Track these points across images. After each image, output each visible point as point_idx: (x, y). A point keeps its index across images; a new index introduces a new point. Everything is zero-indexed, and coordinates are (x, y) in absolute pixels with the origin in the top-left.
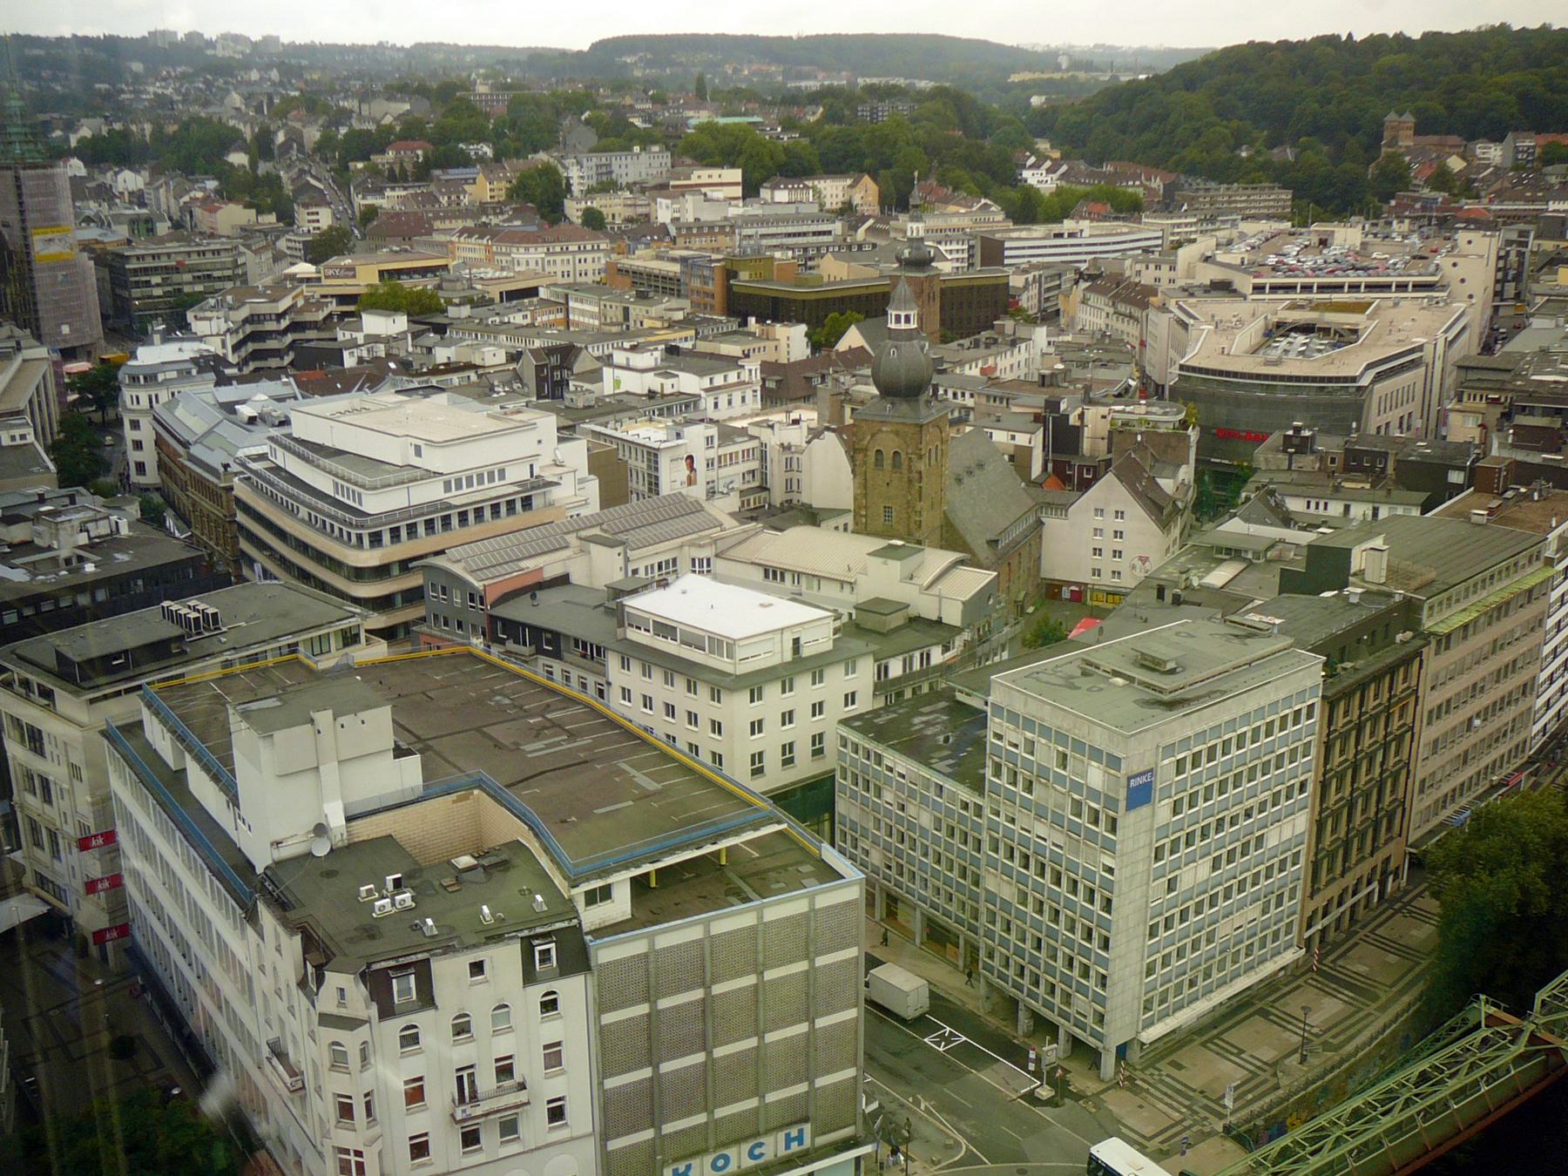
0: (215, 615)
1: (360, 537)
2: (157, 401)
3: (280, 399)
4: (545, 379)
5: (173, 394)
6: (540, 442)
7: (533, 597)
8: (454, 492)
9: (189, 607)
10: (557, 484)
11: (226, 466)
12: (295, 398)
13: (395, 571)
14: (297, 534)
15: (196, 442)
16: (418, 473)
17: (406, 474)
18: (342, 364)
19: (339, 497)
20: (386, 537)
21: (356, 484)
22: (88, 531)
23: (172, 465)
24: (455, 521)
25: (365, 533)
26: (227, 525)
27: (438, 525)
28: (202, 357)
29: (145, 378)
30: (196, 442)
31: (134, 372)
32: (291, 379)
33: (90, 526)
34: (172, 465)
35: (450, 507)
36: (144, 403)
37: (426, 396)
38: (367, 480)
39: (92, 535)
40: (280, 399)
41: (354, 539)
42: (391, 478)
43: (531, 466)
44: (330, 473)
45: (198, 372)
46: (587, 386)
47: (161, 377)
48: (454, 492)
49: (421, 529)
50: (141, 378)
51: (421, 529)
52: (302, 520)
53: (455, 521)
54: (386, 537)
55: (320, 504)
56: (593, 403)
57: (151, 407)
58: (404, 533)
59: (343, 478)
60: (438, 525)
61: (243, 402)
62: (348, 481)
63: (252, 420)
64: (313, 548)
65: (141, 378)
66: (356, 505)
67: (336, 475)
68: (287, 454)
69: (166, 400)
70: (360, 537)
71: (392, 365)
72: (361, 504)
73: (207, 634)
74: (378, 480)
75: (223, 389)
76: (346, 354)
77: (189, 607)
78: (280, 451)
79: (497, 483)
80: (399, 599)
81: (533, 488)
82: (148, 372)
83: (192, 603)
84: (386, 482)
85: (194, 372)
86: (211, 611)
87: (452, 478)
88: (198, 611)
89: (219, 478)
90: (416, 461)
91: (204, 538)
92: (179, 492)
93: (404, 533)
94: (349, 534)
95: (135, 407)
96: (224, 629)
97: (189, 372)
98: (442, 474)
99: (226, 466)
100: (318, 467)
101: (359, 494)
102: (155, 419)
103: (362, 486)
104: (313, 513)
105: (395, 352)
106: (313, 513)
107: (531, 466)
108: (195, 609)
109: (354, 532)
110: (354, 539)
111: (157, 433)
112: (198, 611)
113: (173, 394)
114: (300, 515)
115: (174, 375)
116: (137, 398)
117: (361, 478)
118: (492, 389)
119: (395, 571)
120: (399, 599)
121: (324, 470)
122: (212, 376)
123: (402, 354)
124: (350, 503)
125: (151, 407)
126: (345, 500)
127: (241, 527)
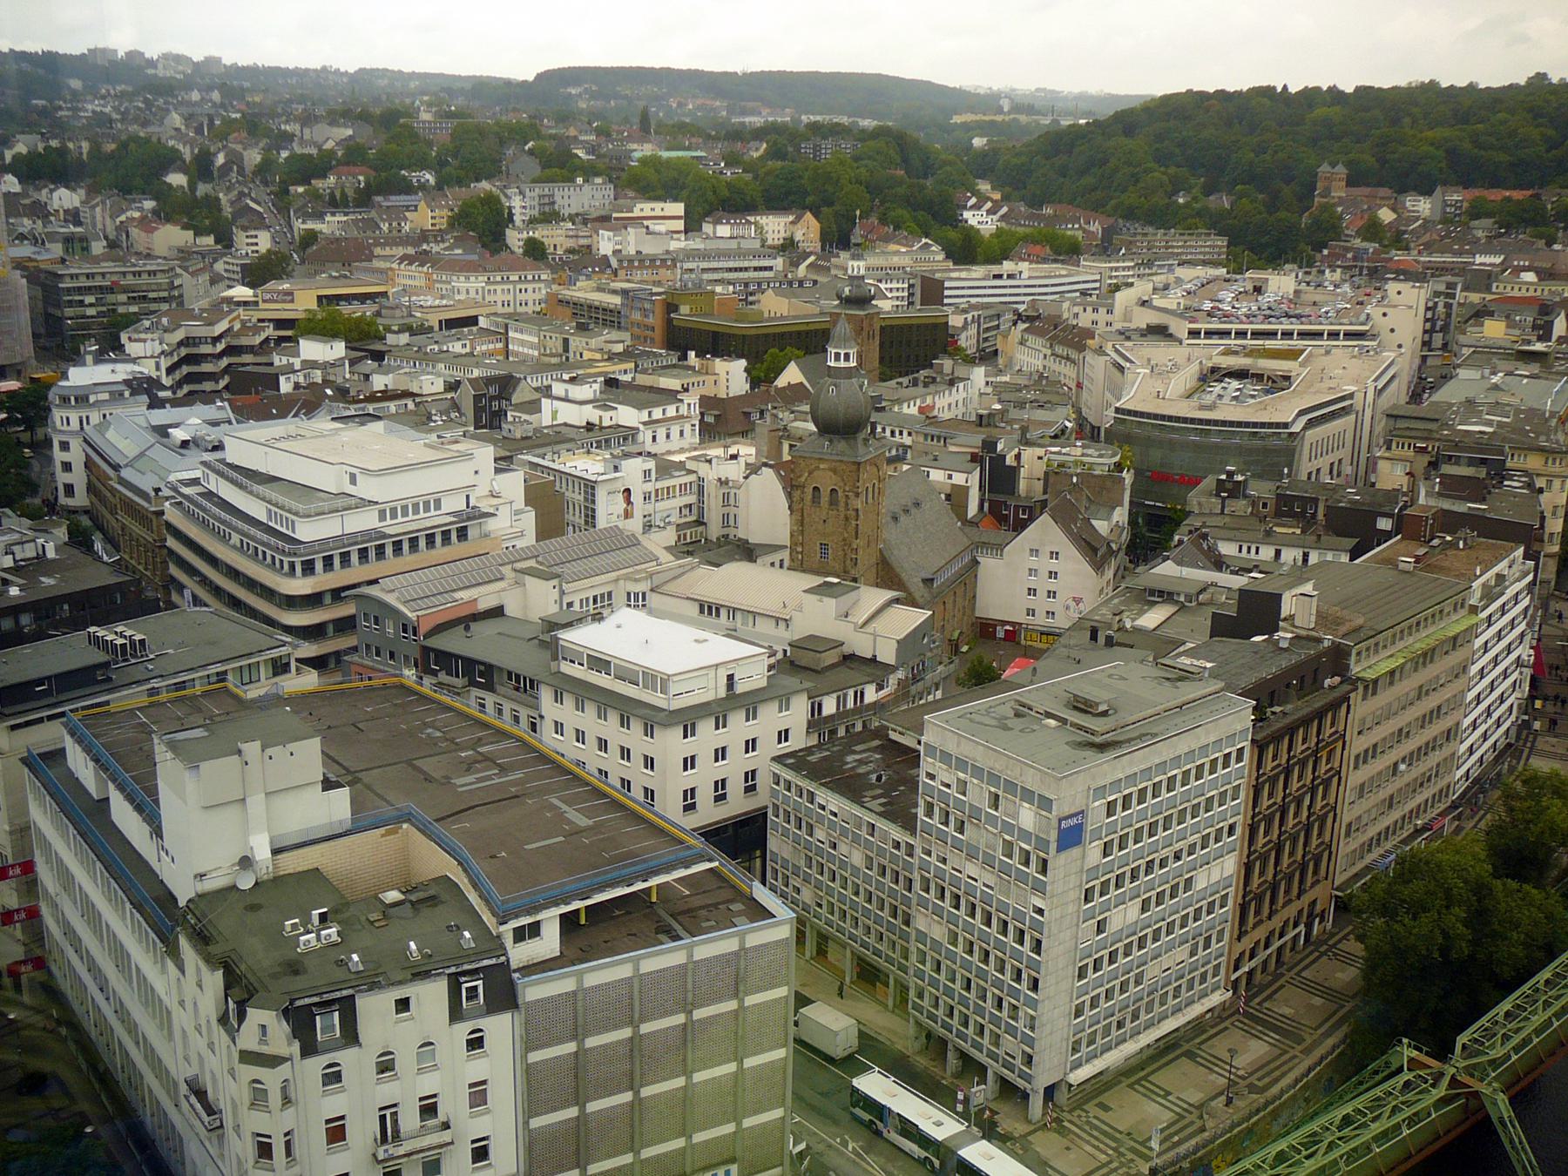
0: (142, 642)
1: (292, 566)
2: (88, 423)
3: (215, 424)
4: (483, 409)
5: (104, 416)
6: (476, 472)
7: (467, 628)
8: (389, 522)
9: (116, 633)
10: (494, 515)
11: (157, 490)
12: (230, 422)
13: (328, 599)
14: (229, 562)
15: (126, 466)
16: (353, 501)
17: (340, 503)
18: (278, 390)
19: (272, 524)
20: (319, 566)
21: (289, 511)
22: (13, 554)
23: (103, 489)
24: (389, 550)
25: (298, 560)
26: (157, 550)
27: (372, 554)
28: (135, 378)
29: (76, 399)
30: (126, 466)
31: (65, 393)
32: (226, 403)
33: (16, 549)
34: (103, 489)
35: (385, 536)
36: (75, 425)
37: (362, 424)
38: (301, 507)
39: (18, 558)
40: (215, 424)
41: (286, 567)
42: (325, 506)
43: (468, 497)
44: (263, 499)
45: (131, 395)
46: (525, 417)
47: (92, 399)
48: (389, 522)
49: (355, 558)
50: (72, 399)
51: (355, 558)
52: (234, 547)
53: (389, 550)
54: (319, 566)
55: (253, 531)
56: (530, 434)
57: (82, 428)
58: (337, 561)
59: (276, 505)
60: (372, 554)
61: (176, 426)
62: (282, 508)
63: (185, 444)
64: (245, 576)
65: (72, 399)
66: (289, 533)
67: (269, 502)
68: (220, 479)
69: (97, 422)
70: (292, 566)
71: (329, 392)
72: (294, 532)
73: (133, 661)
74: (313, 507)
75: (156, 411)
76: (282, 379)
77: (116, 633)
78: (213, 476)
79: (433, 513)
80: (330, 628)
81: (469, 519)
82: (80, 393)
83: (119, 629)
84: (320, 510)
85: (127, 394)
86: (138, 637)
87: (387, 507)
88: (125, 637)
89: (150, 502)
90: (350, 489)
91: (133, 562)
92: (108, 516)
93: (337, 561)
94: (281, 561)
95: (65, 428)
96: (152, 656)
97: (121, 394)
98: (377, 503)
99: (157, 490)
100: (251, 493)
101: (293, 522)
102: (85, 440)
103: (296, 514)
104: (245, 540)
105: (332, 378)
106: (245, 540)
107: (468, 497)
108: (122, 635)
109: (286, 560)
110: (286, 567)
111: (87, 455)
112: (125, 637)
113: (104, 416)
114: (232, 542)
115: (106, 396)
116: (68, 419)
117: (294, 505)
118: (429, 418)
119: (328, 599)
120: (330, 628)
121: (257, 496)
122: (145, 398)
123: (340, 380)
124: (283, 530)
125: (82, 428)
126: (278, 527)
127: (171, 552)
